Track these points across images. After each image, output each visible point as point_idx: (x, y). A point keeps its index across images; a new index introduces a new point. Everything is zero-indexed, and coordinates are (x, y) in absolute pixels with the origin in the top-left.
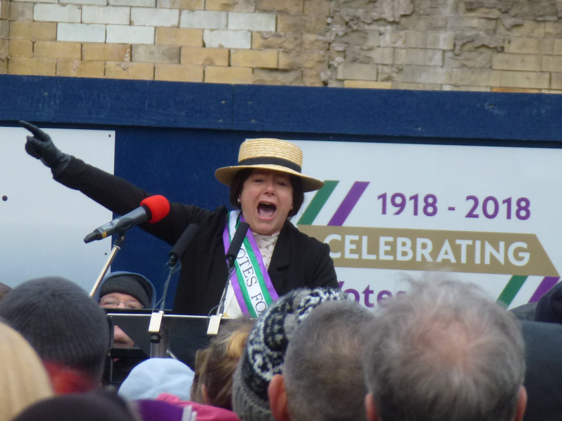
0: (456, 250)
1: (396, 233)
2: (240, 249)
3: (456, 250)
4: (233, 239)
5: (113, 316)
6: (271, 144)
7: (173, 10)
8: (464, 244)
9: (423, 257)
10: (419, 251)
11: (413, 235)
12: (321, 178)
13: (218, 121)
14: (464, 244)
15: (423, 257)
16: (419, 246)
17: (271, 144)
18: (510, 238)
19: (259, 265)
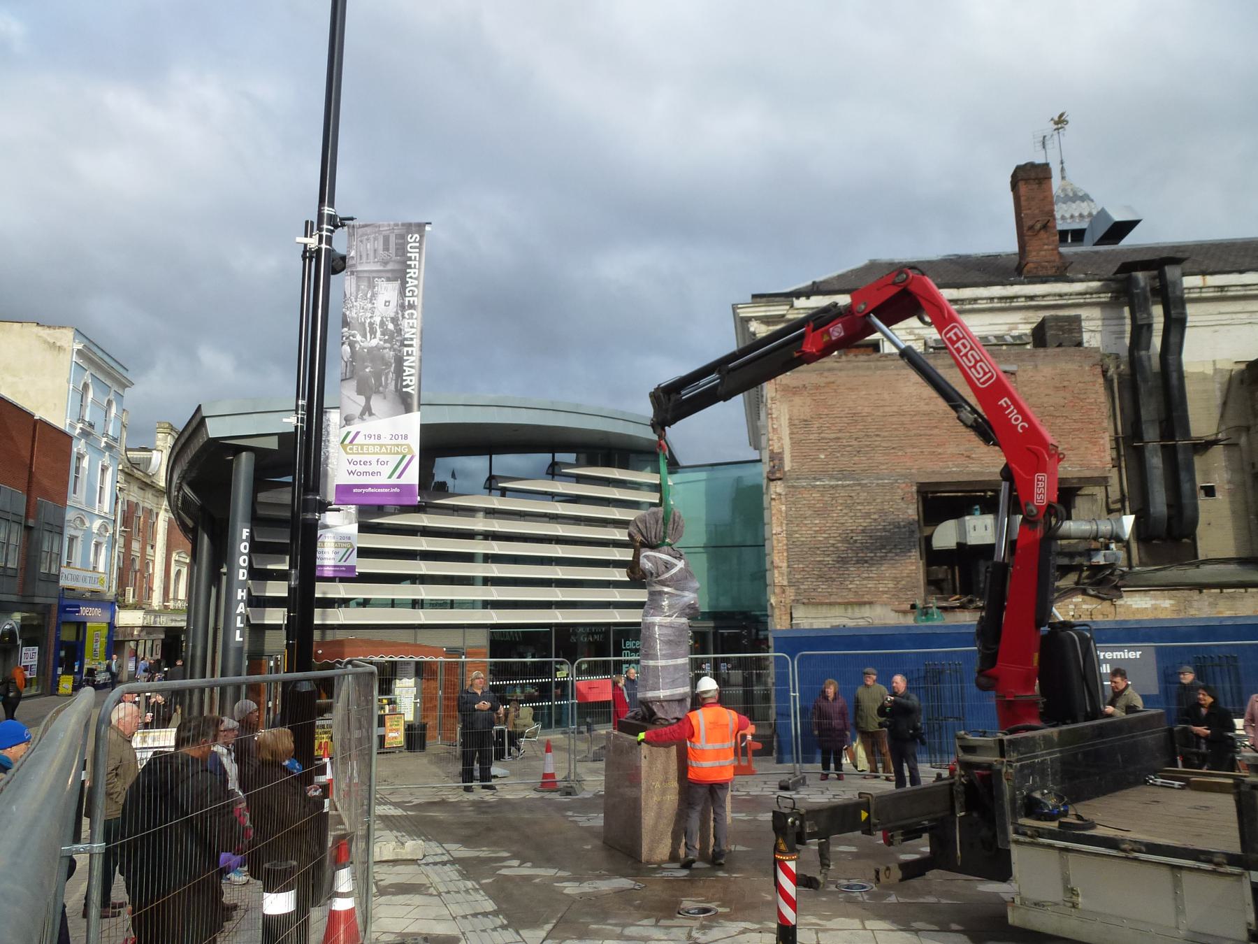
0: (387, 449)
1: (369, 445)
2: (764, 509)
3: (387, 449)
4: (1001, 780)
5: (756, 657)
6: (373, 474)
7: (83, 690)
8: (389, 447)
9: (406, 380)
10: (409, 378)
11: (374, 445)
12: (373, 412)
13: (239, 877)
14: (389, 447)
15: (406, 380)
16: (411, 378)
17: (373, 474)
18: (402, 445)
19: (1253, 597)
